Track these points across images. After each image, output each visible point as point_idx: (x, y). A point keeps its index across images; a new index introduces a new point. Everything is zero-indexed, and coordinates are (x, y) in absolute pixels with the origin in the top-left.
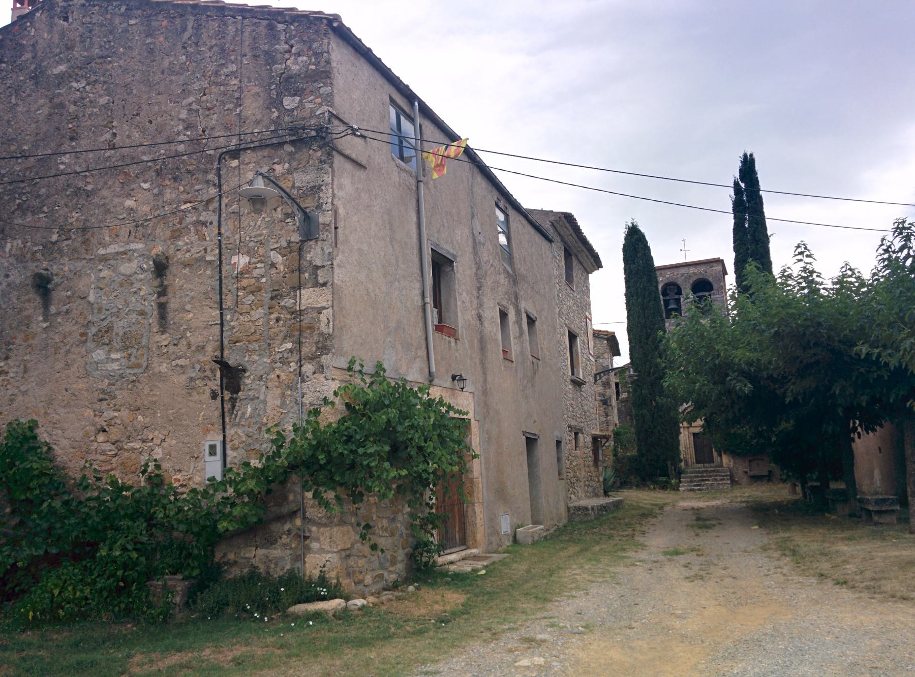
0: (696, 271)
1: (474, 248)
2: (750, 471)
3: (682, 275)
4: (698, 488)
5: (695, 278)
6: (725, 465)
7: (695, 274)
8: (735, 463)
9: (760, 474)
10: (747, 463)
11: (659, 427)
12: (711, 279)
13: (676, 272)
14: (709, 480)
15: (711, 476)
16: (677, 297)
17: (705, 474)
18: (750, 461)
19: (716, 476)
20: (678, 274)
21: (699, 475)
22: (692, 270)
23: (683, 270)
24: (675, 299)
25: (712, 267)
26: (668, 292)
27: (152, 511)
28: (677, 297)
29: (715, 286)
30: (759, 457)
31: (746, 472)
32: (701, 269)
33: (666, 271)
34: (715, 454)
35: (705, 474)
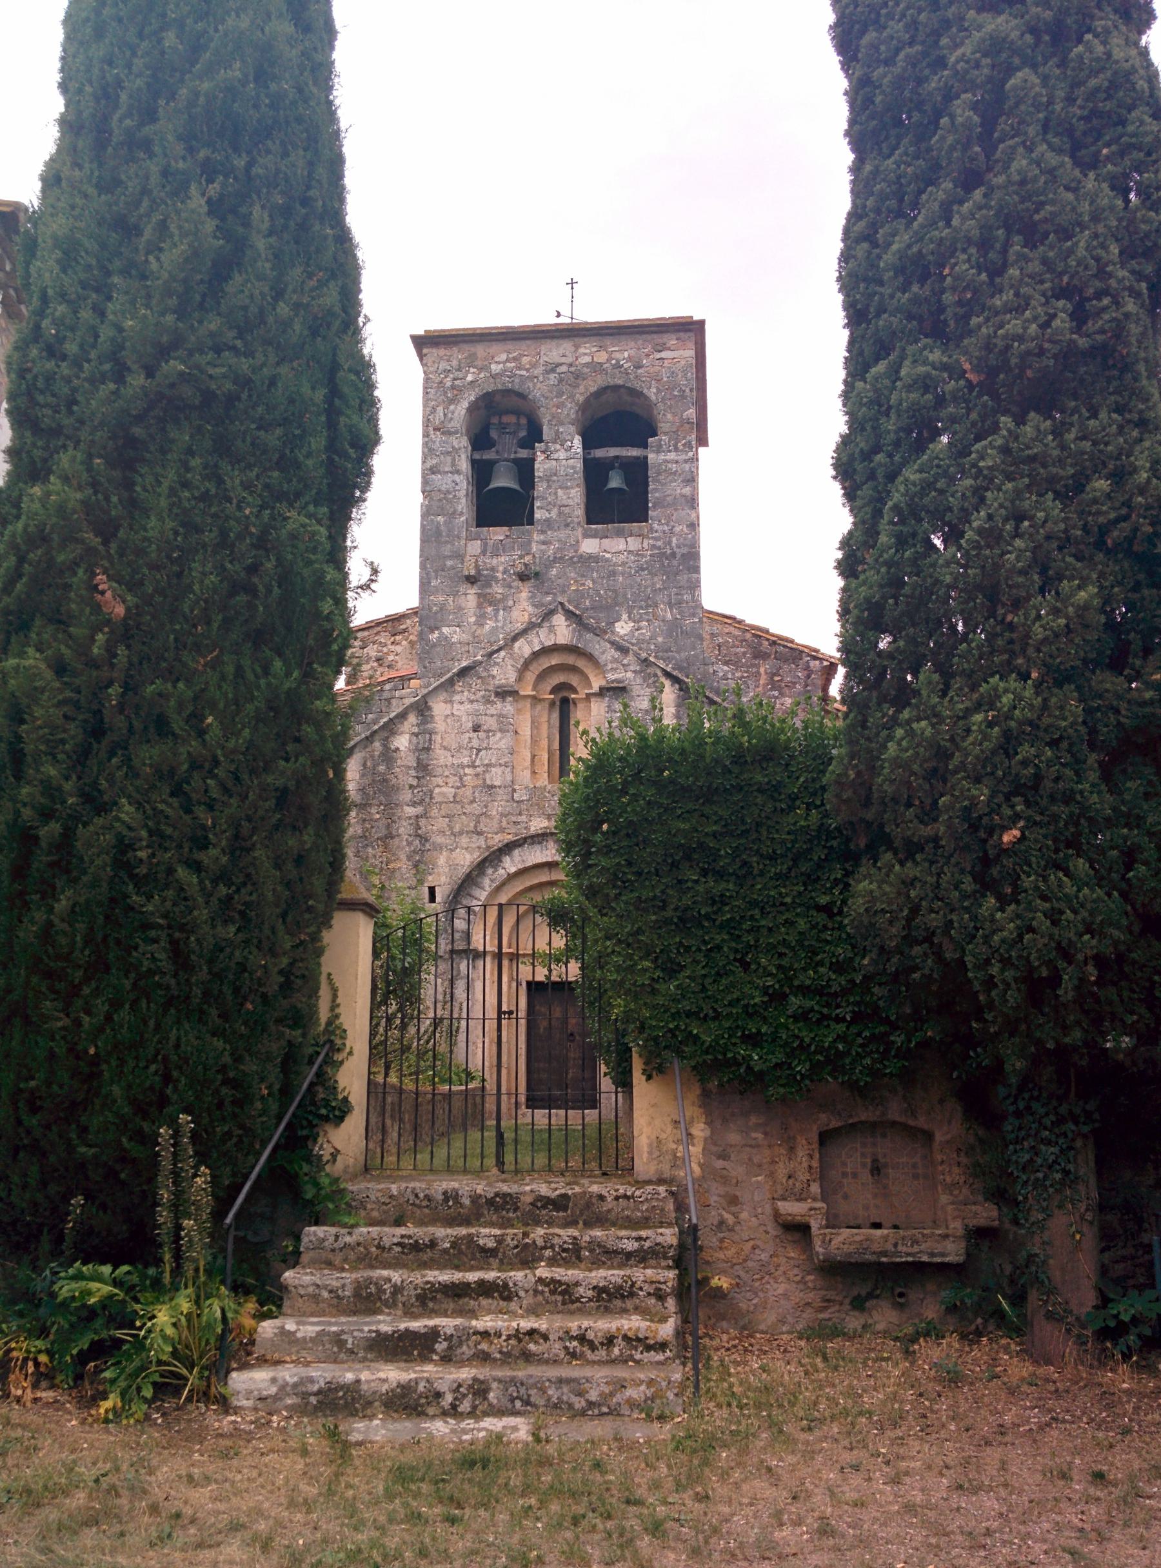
0: (602, 357)
1: (464, 882)
2: (832, 1222)
3: (552, 368)
4: (392, 1374)
5: (592, 385)
6: (644, 1165)
7: (596, 367)
8: (717, 1150)
9: (906, 1253)
10: (804, 1157)
11: (127, 811)
12: (652, 393)
13: (527, 354)
14: (503, 1292)
15: (527, 1257)
16: (523, 454)
17: (486, 1235)
18: (825, 1138)
19: (572, 1255)
20: (534, 366)
21: (444, 1234)
22: (587, 353)
23: (554, 352)
24: (517, 462)
25: (663, 347)
26: (494, 434)
27: (173, 1011)
28: (523, 454)
29: (666, 420)
30: (895, 1111)
31: (798, 1230)
32: (624, 352)
33: (495, 348)
34: (606, 1084)
35: (486, 1235)
